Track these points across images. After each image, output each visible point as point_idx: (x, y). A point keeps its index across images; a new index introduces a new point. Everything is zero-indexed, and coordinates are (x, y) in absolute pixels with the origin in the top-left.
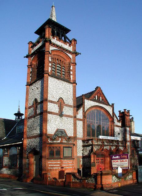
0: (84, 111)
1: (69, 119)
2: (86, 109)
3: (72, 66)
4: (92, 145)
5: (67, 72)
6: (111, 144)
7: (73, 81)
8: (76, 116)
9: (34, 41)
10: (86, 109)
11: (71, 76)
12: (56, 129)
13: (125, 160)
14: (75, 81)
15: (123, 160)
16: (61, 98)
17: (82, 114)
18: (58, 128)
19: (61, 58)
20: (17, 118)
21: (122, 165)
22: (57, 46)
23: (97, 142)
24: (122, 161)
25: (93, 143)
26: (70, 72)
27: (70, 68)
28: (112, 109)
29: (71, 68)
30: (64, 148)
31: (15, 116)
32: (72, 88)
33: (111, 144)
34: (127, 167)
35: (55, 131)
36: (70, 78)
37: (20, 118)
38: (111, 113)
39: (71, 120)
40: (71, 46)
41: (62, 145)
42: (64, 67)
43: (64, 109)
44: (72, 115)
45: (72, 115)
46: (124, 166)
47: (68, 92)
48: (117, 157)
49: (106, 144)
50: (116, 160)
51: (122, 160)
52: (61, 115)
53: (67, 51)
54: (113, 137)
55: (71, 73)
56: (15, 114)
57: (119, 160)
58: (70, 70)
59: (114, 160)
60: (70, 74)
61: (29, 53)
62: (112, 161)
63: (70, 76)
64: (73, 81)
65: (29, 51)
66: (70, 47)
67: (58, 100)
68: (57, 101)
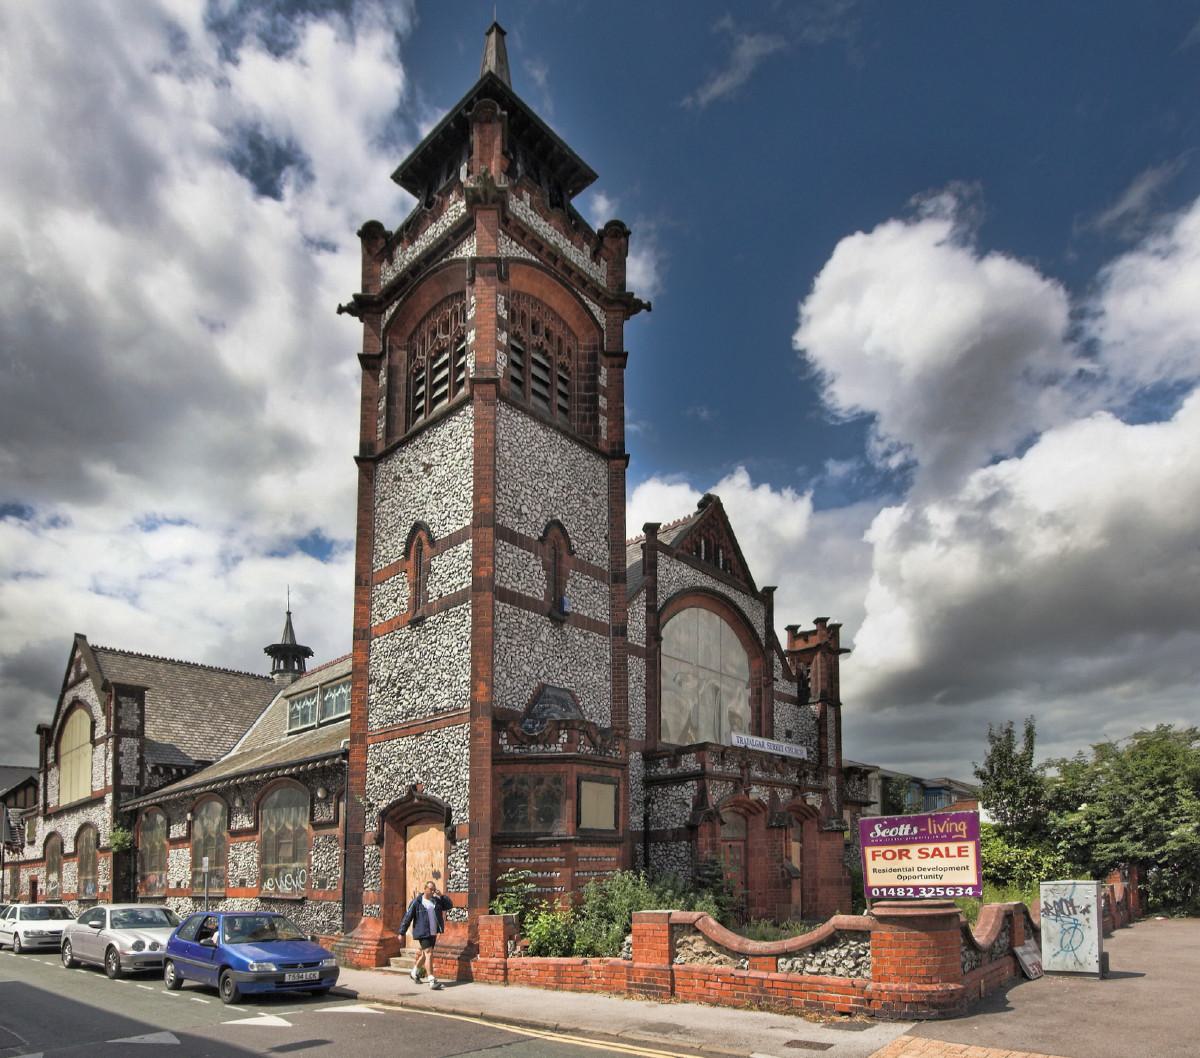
0: (651, 609)
1: (591, 640)
2: (661, 600)
3: (604, 371)
4: (700, 776)
5: (584, 400)
6: (777, 776)
7: (613, 444)
8: (625, 629)
9: (393, 223)
10: (661, 600)
11: (603, 422)
12: (534, 685)
13: (953, 847)
14: (622, 444)
15: (942, 847)
16: (558, 524)
17: (643, 621)
18: (544, 680)
19: (547, 322)
20: (282, 667)
21: (931, 873)
22: (537, 244)
23: (723, 764)
24: (937, 853)
25: (703, 767)
26: (595, 400)
27: (595, 378)
28: (762, 611)
29: (603, 381)
30: (584, 784)
31: (269, 659)
32: (604, 480)
33: (777, 776)
34: (965, 887)
35: (528, 694)
36: (597, 430)
37: (296, 667)
38: (761, 631)
39: (604, 645)
40: (602, 261)
41: (575, 767)
42: (563, 367)
43: (569, 586)
44: (605, 619)
45: (605, 619)
46: (943, 882)
47: (590, 498)
48: (904, 830)
49: (759, 774)
50: (896, 849)
51: (931, 848)
52: (556, 613)
53: (584, 281)
54: (766, 741)
55: (603, 402)
56: (273, 651)
57: (914, 849)
58: (593, 386)
59: (883, 849)
60: (596, 408)
61: (365, 287)
62: (869, 851)
63: (595, 418)
64: (613, 444)
65: (368, 276)
66: (598, 264)
67: (545, 533)
68: (540, 539)
